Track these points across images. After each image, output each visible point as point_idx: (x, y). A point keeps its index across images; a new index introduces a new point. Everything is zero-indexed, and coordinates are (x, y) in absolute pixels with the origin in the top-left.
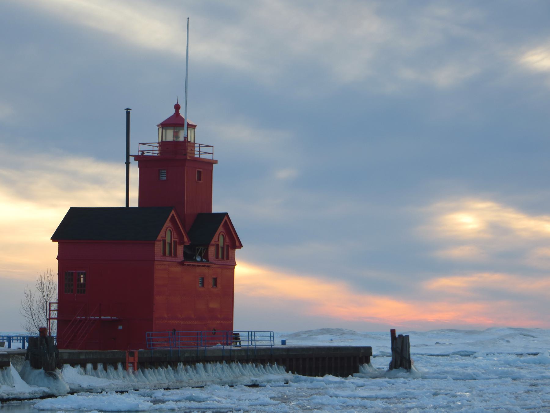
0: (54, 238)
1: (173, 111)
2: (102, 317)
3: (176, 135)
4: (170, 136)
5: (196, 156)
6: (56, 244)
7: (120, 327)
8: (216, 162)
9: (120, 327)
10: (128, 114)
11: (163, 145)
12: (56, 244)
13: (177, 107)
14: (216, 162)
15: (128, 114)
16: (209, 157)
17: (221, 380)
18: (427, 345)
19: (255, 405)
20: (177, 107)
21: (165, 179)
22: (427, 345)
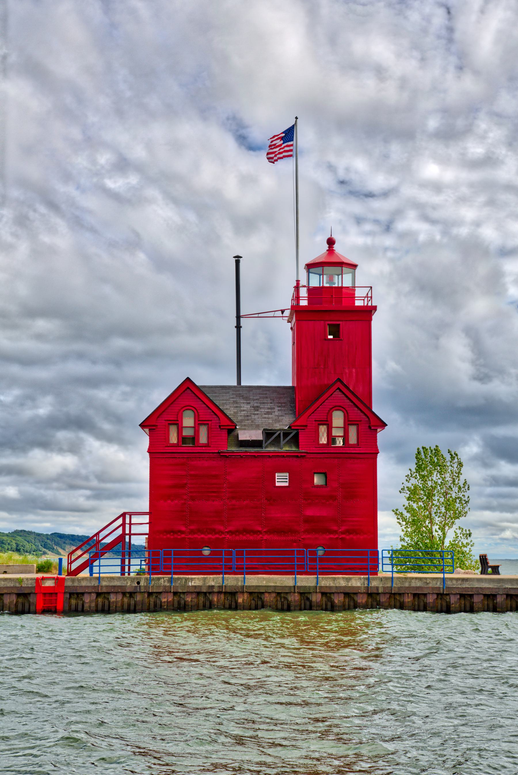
1: (326, 247)
8: (375, 308)
10: (237, 263)
13: (331, 242)
15: (237, 263)
20: (331, 242)
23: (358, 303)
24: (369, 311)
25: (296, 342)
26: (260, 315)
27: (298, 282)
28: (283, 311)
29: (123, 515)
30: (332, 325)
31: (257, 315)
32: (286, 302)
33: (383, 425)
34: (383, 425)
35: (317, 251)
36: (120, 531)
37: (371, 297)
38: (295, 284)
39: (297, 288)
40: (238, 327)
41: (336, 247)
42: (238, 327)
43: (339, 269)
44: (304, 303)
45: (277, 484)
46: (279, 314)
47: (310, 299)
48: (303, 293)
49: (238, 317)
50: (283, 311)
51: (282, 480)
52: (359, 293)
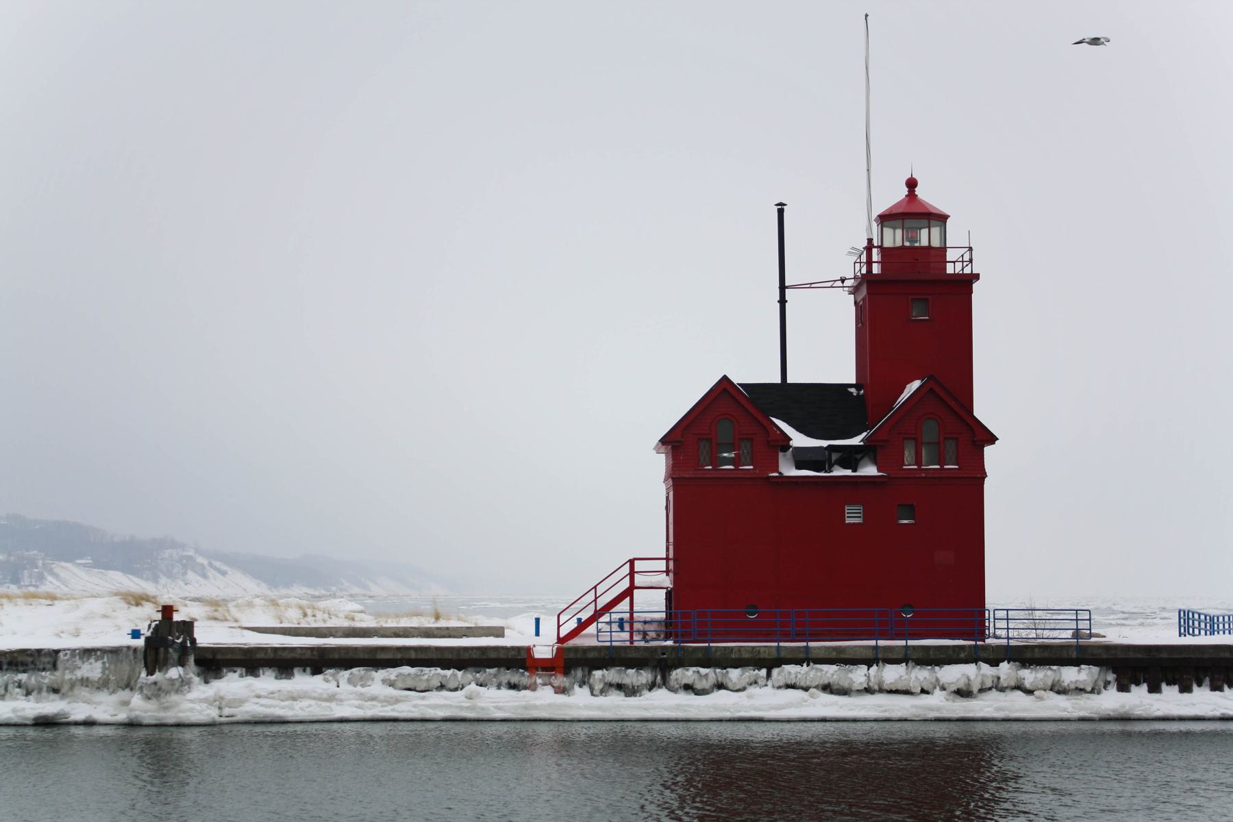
1: (905, 191)
8: (977, 277)
10: (781, 213)
13: (912, 184)
14: (977, 277)
15: (781, 213)
16: (967, 271)
20: (912, 184)
23: (950, 269)
24: (966, 283)
25: (671, 540)
26: (829, 284)
27: (870, 241)
28: (843, 280)
29: (632, 562)
30: (916, 301)
31: (829, 284)
32: (849, 268)
33: (992, 439)
34: (992, 439)
35: (892, 196)
36: (625, 584)
37: (971, 261)
38: (865, 244)
39: (869, 248)
40: (783, 302)
41: (918, 191)
42: (783, 302)
43: (925, 222)
44: (876, 269)
45: (848, 521)
46: (839, 284)
47: (882, 263)
48: (876, 256)
49: (783, 288)
50: (843, 280)
51: (853, 516)
52: (951, 255)
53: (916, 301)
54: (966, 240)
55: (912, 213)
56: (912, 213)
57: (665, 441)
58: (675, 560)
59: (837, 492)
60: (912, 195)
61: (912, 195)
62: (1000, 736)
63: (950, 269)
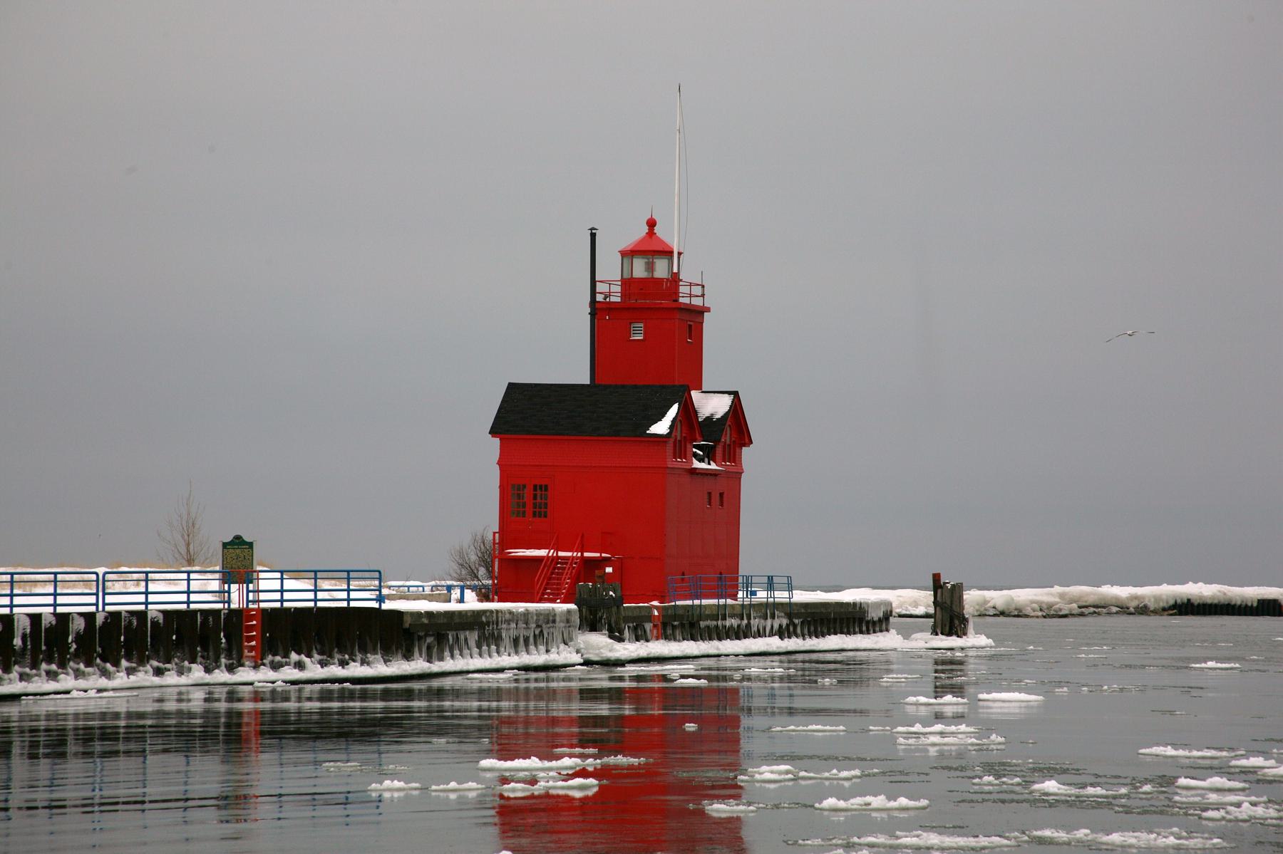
0: (494, 431)
1: (646, 229)
2: (586, 554)
3: (650, 267)
4: (639, 269)
5: (681, 300)
6: (497, 441)
7: (609, 570)
8: (708, 310)
9: (609, 570)
10: (593, 236)
11: (628, 284)
12: (497, 441)
13: (652, 224)
14: (708, 310)
15: (593, 236)
16: (697, 302)
17: (952, 602)
18: (145, 844)
19: (952, 649)
20: (652, 224)
21: (640, 337)
22: (145, 844)
24: (700, 312)
41: (656, 229)
52: (683, 289)
53: (649, 325)
54: (701, 271)
55: (651, 247)
56: (651, 247)
57: (511, 387)
58: (348, 609)
59: (617, 450)
60: (651, 233)
61: (651, 233)
62: (738, 819)
63: (681, 300)
